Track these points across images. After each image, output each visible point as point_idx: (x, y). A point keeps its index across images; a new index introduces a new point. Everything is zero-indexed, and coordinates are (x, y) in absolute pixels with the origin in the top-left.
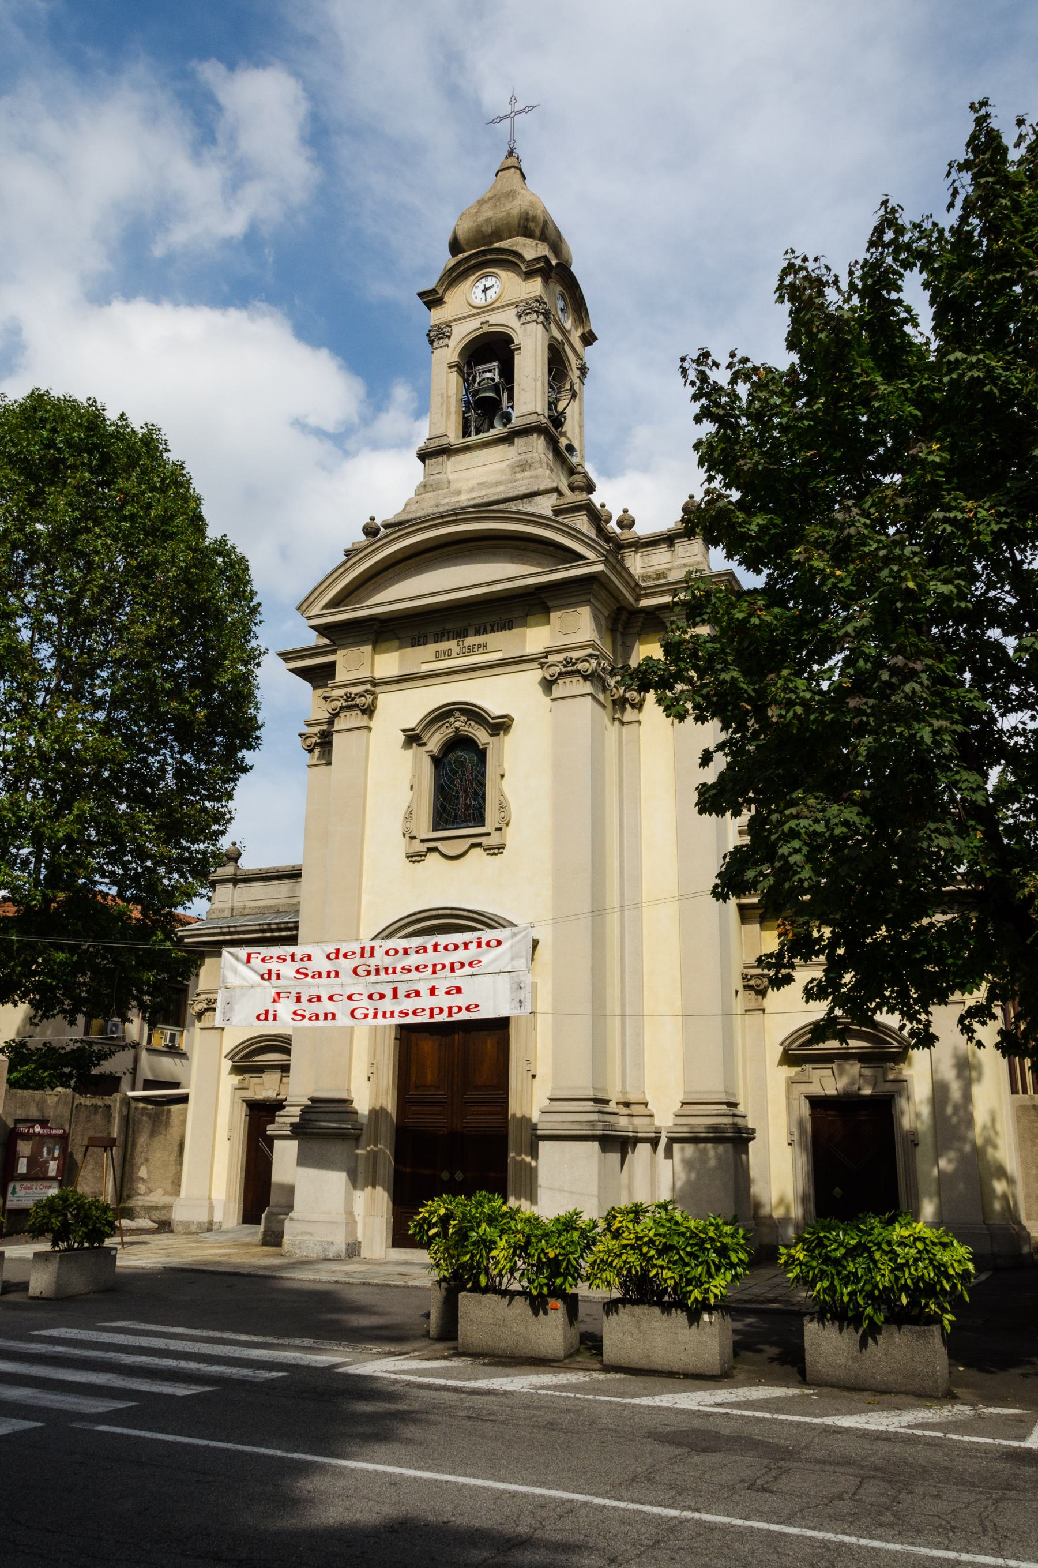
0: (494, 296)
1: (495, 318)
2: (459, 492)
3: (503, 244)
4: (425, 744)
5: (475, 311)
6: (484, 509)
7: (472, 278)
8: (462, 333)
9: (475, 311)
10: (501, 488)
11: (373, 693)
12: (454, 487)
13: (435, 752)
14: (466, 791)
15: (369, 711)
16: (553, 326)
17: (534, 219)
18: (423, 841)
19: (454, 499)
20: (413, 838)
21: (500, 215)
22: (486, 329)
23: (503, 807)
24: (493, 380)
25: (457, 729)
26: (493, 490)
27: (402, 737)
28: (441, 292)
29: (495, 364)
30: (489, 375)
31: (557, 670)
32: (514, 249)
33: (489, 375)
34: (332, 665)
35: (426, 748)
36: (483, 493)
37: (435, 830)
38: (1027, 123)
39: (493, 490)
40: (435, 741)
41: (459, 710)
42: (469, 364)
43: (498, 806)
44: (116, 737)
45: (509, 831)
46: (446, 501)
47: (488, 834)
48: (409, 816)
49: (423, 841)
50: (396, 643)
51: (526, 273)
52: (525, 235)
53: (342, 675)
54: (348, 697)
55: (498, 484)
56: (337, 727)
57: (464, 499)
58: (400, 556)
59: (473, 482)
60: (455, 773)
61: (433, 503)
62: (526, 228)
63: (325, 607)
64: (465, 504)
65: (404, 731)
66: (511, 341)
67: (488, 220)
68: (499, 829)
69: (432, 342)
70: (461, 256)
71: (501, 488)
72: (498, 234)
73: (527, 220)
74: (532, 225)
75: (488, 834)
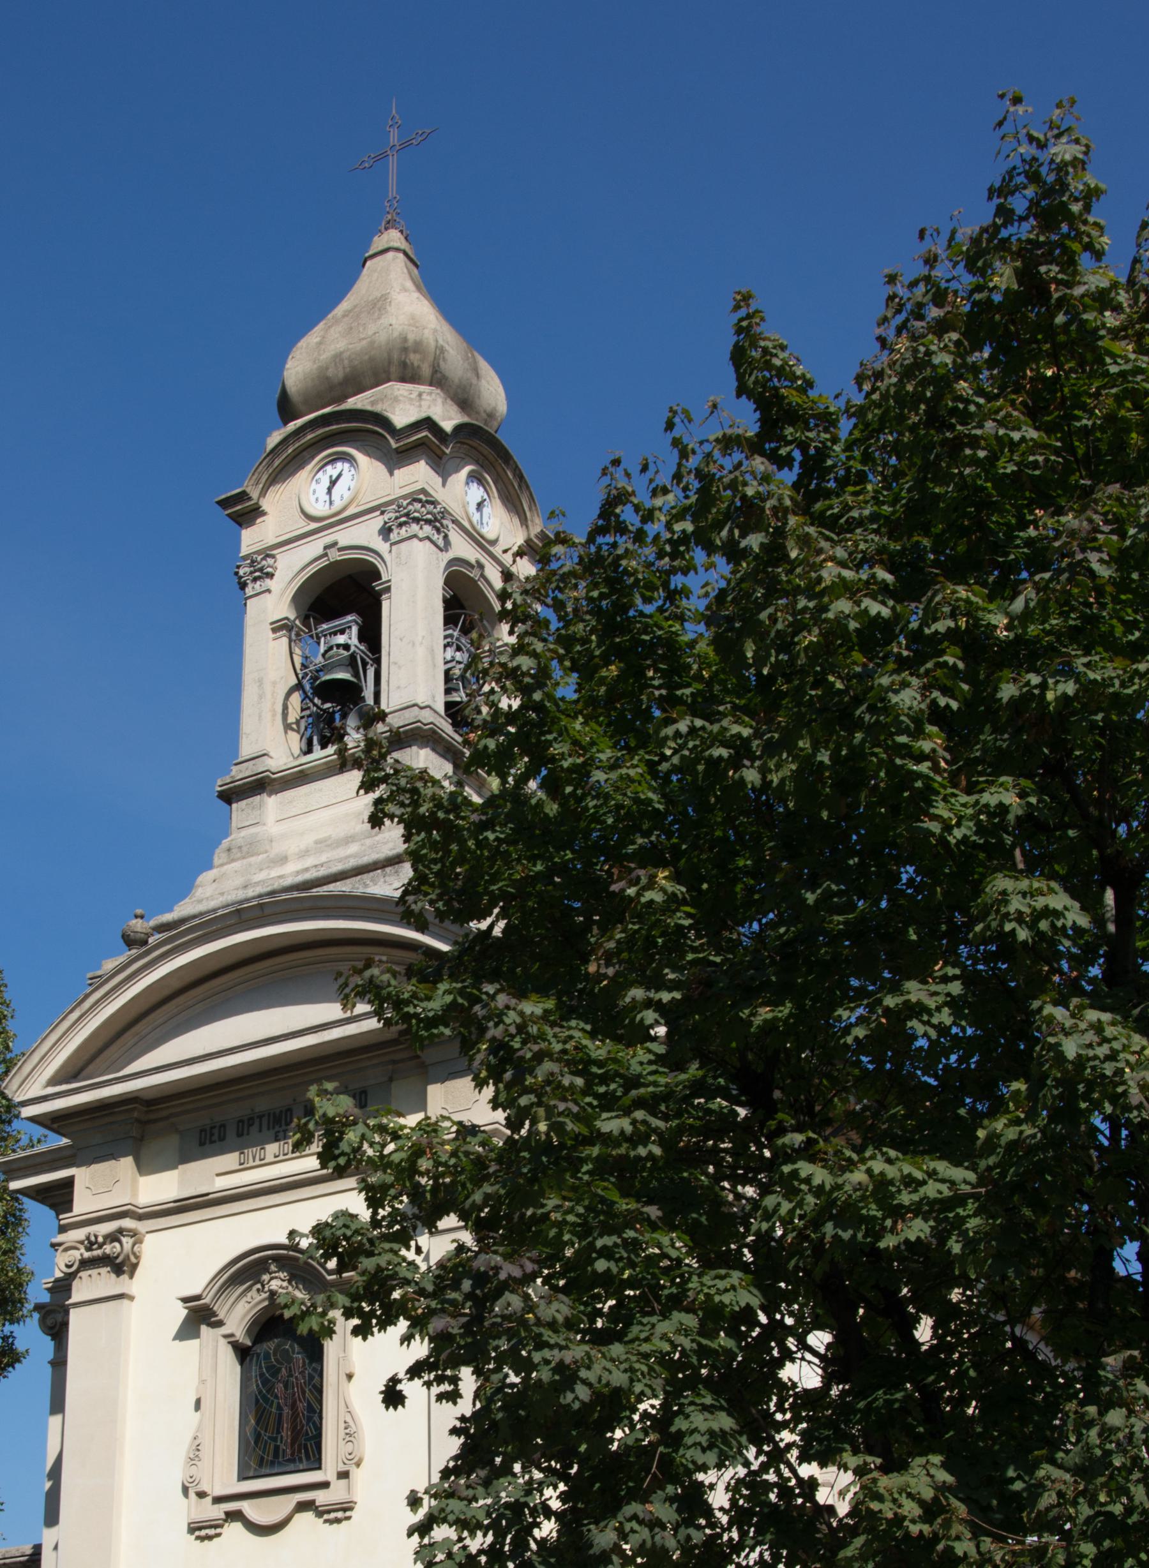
0: (347, 495)
1: (346, 536)
2: (283, 860)
3: (355, 402)
4: (220, 1324)
5: (314, 525)
6: (302, 899)
7: (309, 467)
8: (292, 568)
9: (314, 525)
10: (353, 848)
11: (134, 1234)
12: (276, 849)
13: (240, 1335)
14: (293, 1407)
15: (122, 1266)
16: (455, 536)
17: (418, 347)
18: (218, 1500)
19: (274, 873)
20: (201, 1495)
21: (358, 346)
22: (335, 556)
23: (350, 1435)
24: (346, 647)
25: (273, 1294)
26: (342, 852)
27: (181, 1313)
28: (255, 494)
29: (349, 618)
30: (341, 639)
31: (76, 1255)
32: (378, 408)
33: (341, 639)
34: (69, 1183)
35: (224, 1330)
36: (323, 858)
37: (242, 1477)
38: (622, 466)
39: (342, 852)
40: (239, 1314)
41: (276, 1259)
42: (305, 620)
43: (342, 1432)
44: (797, 1268)
45: (357, 1474)
46: (262, 876)
47: (325, 1485)
48: (195, 1455)
49: (218, 1500)
50: (174, 1140)
51: (398, 451)
52: (403, 380)
53: (83, 1203)
54: (90, 1244)
55: (348, 840)
56: (76, 1297)
57: (290, 872)
58: (176, 984)
59: (308, 840)
60: (275, 1371)
61: (239, 881)
62: (404, 365)
63: (52, 1082)
64: (288, 882)
65: (185, 1300)
66: (377, 575)
67: (338, 357)
68: (344, 1475)
69: (243, 586)
70: (293, 426)
71: (353, 848)
72: (356, 382)
73: (405, 350)
74: (414, 358)
75: (325, 1485)
